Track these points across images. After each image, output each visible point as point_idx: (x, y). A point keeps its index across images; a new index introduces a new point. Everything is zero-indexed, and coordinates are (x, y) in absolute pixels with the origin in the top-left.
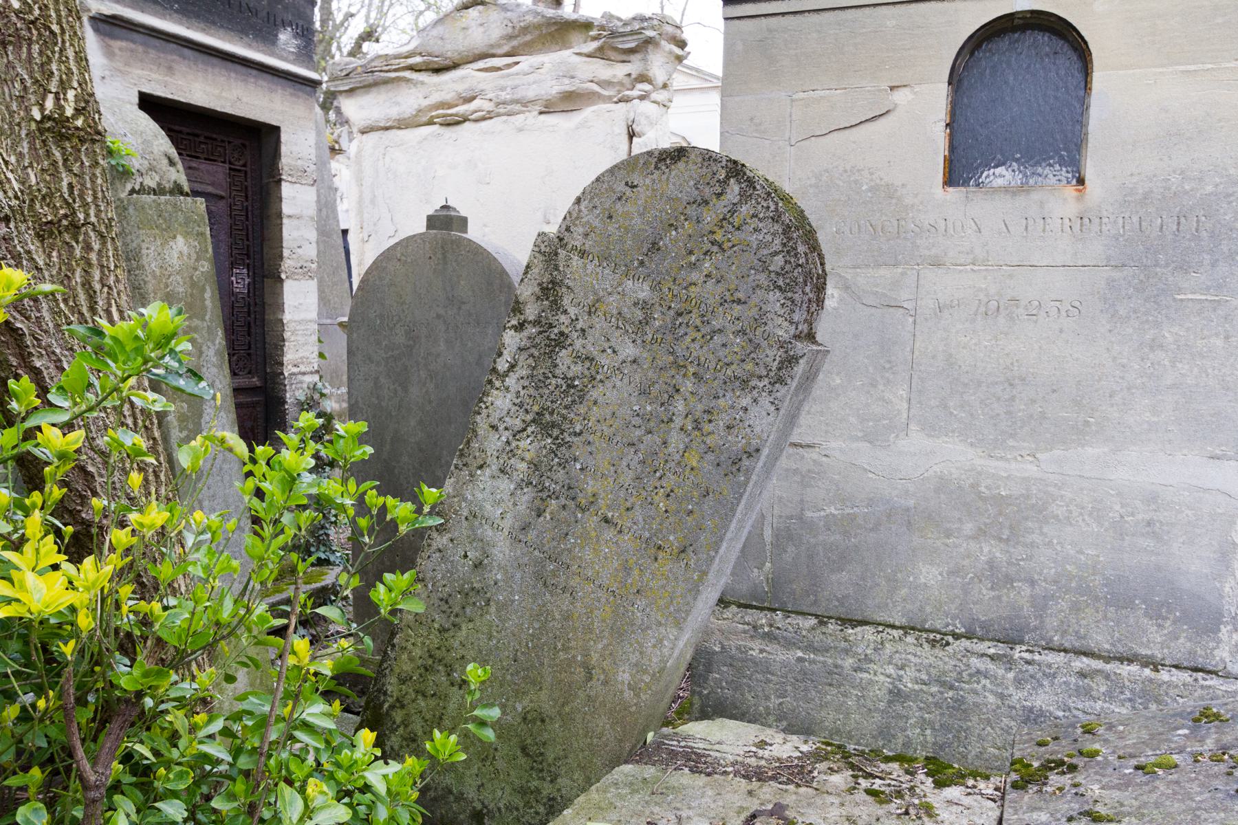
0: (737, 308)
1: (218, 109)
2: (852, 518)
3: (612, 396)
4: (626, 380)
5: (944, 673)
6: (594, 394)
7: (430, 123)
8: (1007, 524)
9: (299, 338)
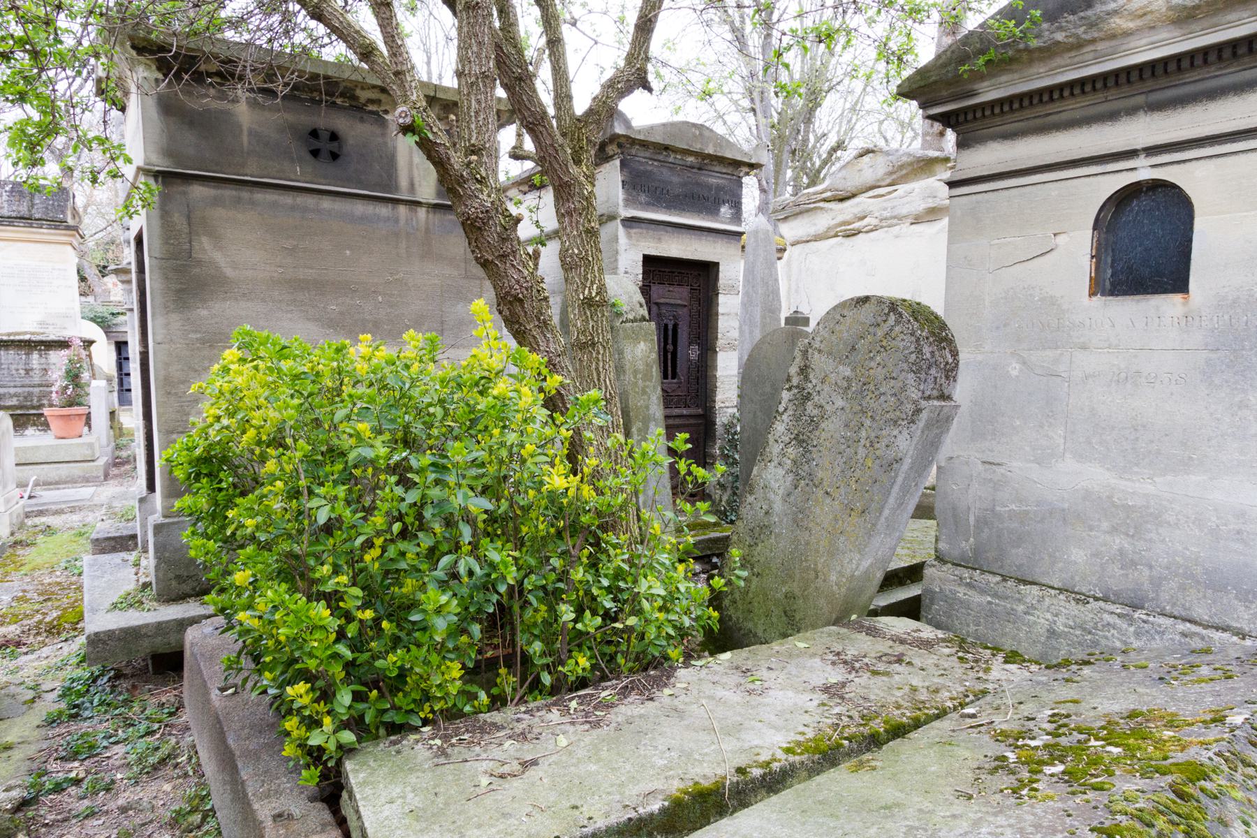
3: (831, 427)
5: (1085, 622)
7: (836, 236)
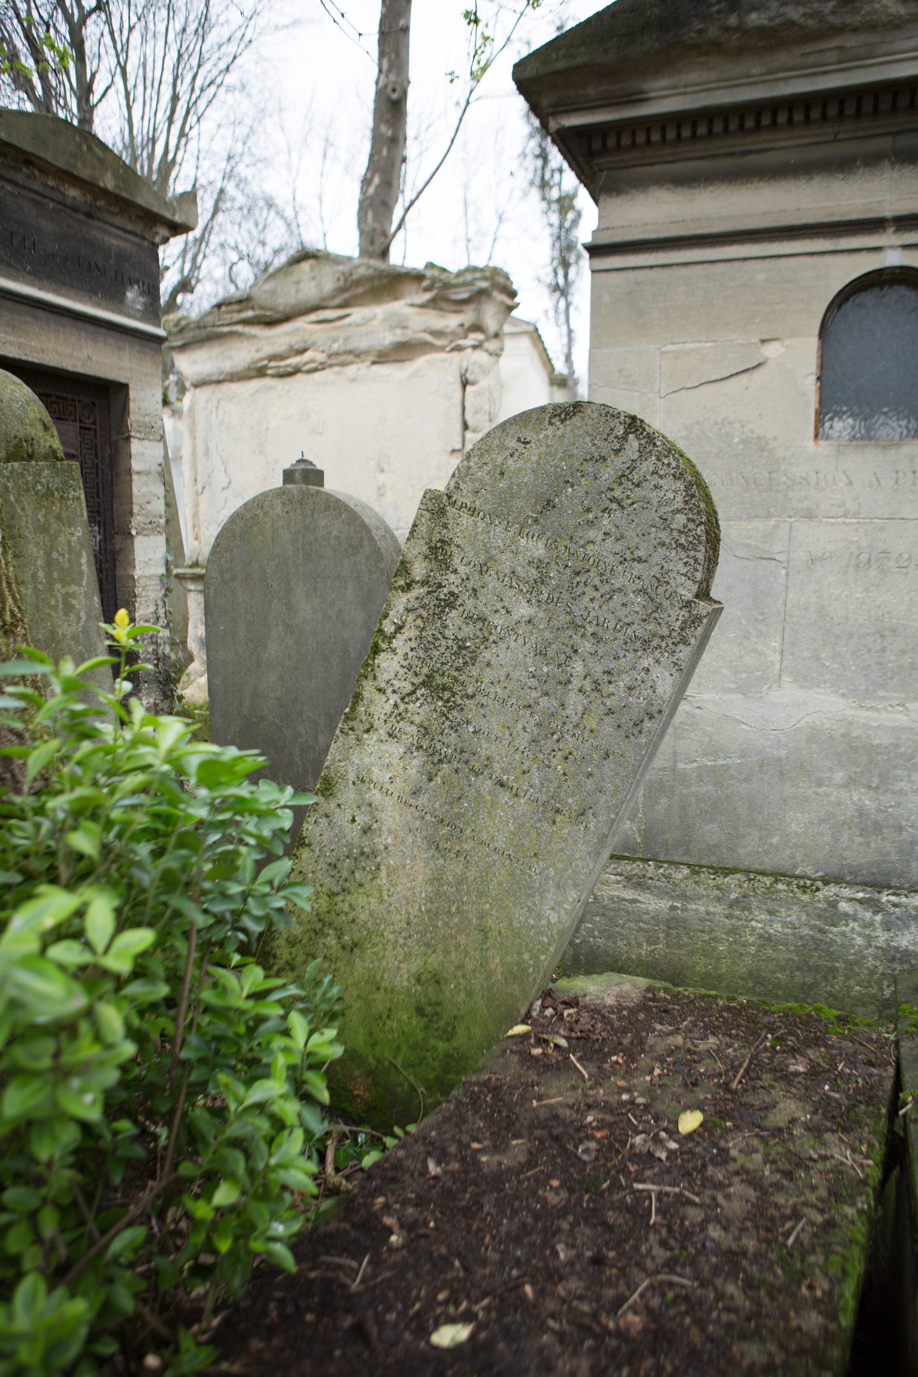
0: (638, 568)
1: (70, 369)
2: (726, 768)
4: (520, 641)
6: (487, 655)
8: (877, 772)
9: (150, 593)
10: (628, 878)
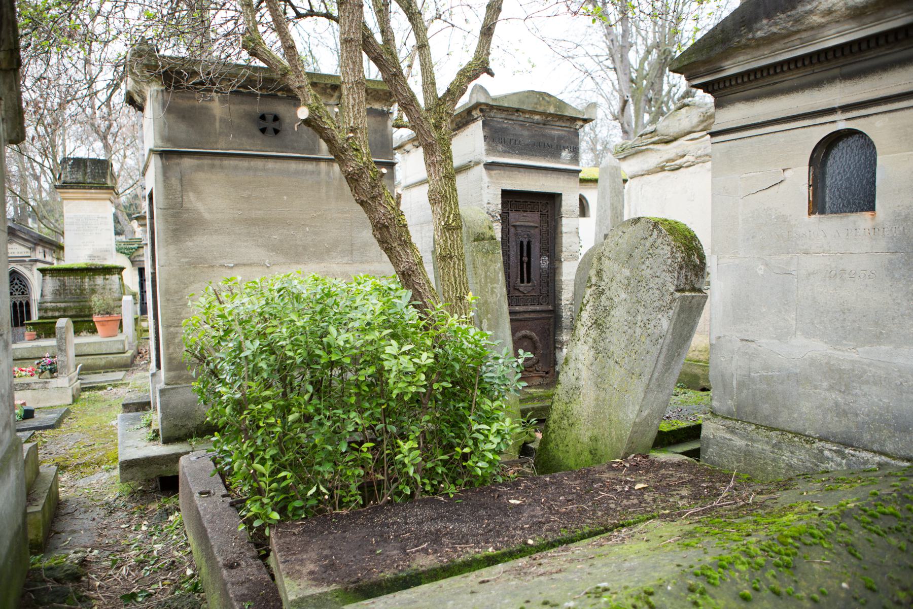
2: (772, 377)
10: (728, 428)
